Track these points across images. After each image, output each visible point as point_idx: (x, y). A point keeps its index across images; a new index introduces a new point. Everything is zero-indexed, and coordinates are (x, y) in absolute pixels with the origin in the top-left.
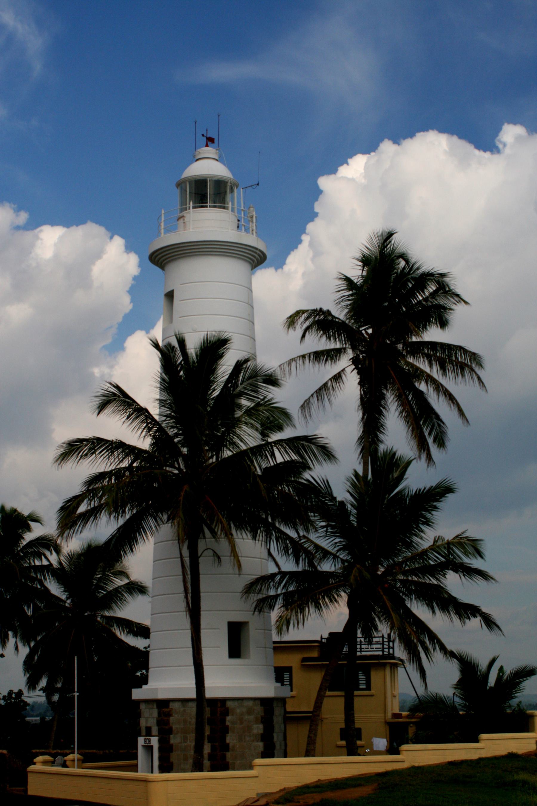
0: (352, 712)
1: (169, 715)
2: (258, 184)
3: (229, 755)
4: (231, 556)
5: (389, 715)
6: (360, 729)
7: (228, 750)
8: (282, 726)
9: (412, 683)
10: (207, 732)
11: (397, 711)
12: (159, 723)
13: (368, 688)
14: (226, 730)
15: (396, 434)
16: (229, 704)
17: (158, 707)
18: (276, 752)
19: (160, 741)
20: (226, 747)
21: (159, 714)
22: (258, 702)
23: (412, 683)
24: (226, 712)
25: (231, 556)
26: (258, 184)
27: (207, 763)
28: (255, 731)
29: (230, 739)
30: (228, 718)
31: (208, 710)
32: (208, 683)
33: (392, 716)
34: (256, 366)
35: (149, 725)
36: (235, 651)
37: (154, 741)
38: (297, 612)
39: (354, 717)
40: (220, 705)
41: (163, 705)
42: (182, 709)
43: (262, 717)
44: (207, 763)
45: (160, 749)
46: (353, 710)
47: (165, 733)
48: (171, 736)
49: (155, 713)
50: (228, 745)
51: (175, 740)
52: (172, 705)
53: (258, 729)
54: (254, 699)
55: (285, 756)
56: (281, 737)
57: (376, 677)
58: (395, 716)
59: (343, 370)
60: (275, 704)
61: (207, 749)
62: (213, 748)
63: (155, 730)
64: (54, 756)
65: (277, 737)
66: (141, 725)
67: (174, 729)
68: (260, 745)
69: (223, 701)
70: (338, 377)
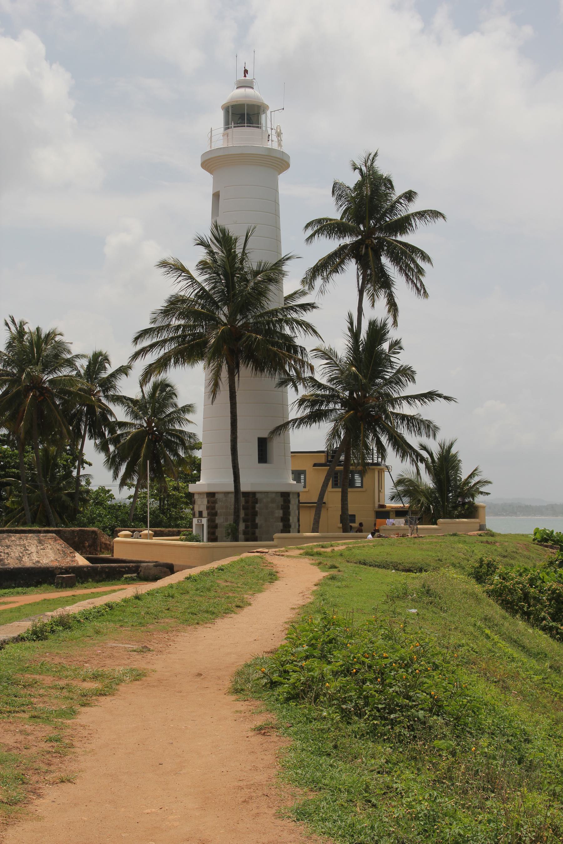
1: (215, 502)
3: (257, 531)
5: (377, 505)
7: (257, 528)
8: (297, 512)
10: (242, 514)
12: (208, 508)
14: (255, 514)
16: (258, 496)
17: (207, 497)
18: (291, 530)
19: (208, 521)
20: (255, 526)
21: (208, 502)
24: (256, 501)
27: (241, 536)
28: (277, 515)
29: (258, 520)
30: (257, 506)
31: (242, 499)
32: (242, 480)
35: (201, 510)
36: (263, 457)
37: (204, 521)
40: (251, 498)
41: (211, 495)
42: (224, 499)
43: (282, 505)
44: (241, 536)
45: (209, 527)
47: (212, 514)
48: (217, 517)
49: (205, 501)
50: (257, 524)
51: (219, 520)
52: (216, 495)
53: (279, 513)
54: (277, 493)
55: (299, 532)
56: (296, 520)
60: (291, 496)
61: (242, 526)
62: (247, 527)
63: (205, 514)
64: (133, 532)
65: (293, 519)
68: (281, 524)
69: (254, 494)
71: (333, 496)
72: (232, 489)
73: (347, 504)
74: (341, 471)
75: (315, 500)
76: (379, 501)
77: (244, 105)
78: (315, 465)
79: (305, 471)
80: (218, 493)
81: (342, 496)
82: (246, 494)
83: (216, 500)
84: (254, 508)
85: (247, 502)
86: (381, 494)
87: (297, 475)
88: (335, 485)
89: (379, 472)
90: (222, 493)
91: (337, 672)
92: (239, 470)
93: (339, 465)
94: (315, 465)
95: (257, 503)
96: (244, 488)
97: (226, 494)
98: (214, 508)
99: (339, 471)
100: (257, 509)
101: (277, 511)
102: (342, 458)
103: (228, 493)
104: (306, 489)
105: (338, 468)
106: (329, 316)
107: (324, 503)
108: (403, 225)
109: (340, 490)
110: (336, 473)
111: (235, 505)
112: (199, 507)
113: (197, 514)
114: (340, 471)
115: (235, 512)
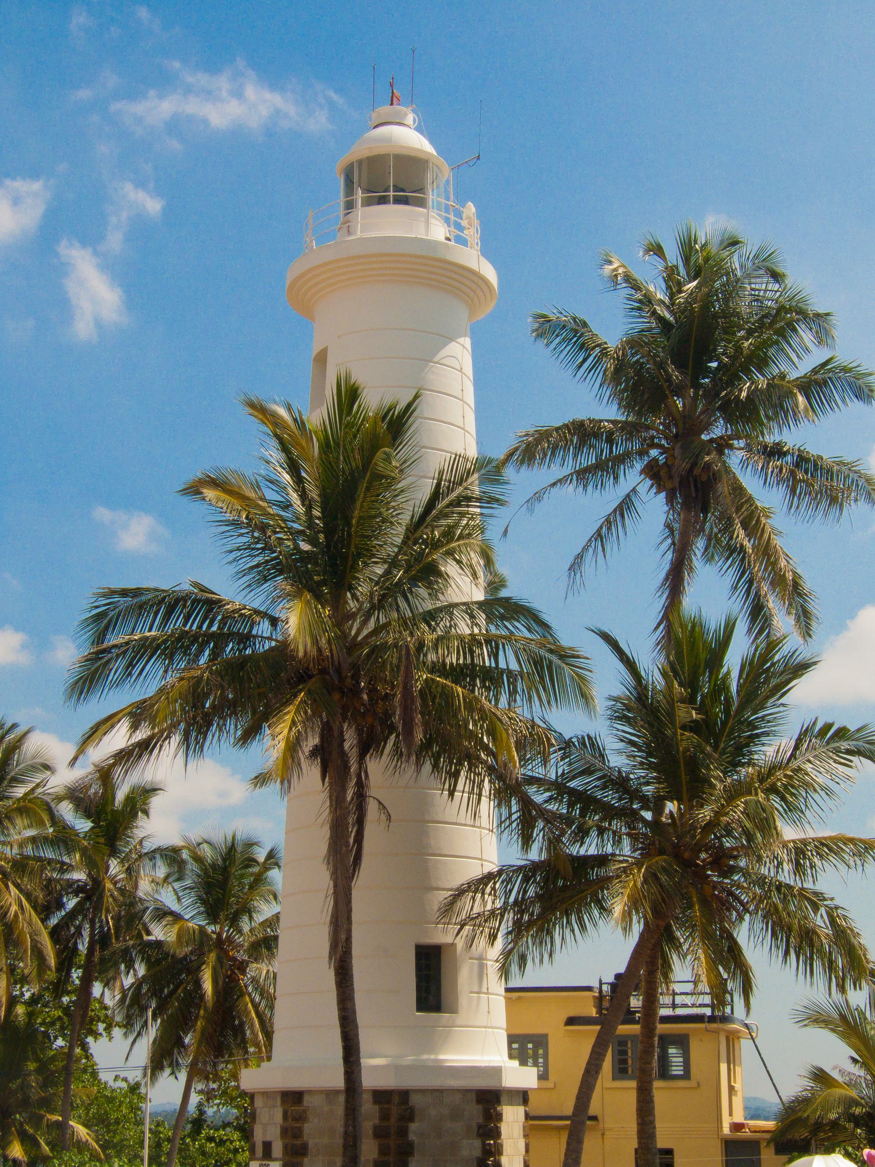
0: (650, 1118)
1: (301, 1118)
2: (478, 158)
4: (497, 961)
5: (726, 1130)
6: (669, 1152)
8: (522, 1144)
9: (768, 1071)
11: (738, 1118)
12: (284, 1132)
13: (686, 1076)
15: (712, 595)
17: (283, 1102)
22: (474, 1096)
23: (766, 1067)
24: (409, 1116)
25: (497, 961)
26: (478, 158)
28: (465, 1153)
30: (413, 1126)
33: (730, 1128)
34: (605, 910)
35: (268, 1139)
38: (438, 662)
39: (655, 1128)
41: (293, 1098)
42: (326, 1109)
43: (480, 1127)
46: (653, 1115)
48: (306, 1160)
52: (307, 1100)
54: (466, 1092)
57: (700, 1049)
58: (737, 1127)
59: (634, 490)
63: (277, 1149)
66: (255, 1139)
67: (310, 1146)
69: (404, 1095)
70: (625, 507)
71: (616, 1099)
72: (338, 1081)
73: (652, 1122)
74: (635, 1036)
75: (569, 1110)
76: (731, 1114)
77: (389, 155)
78: (571, 1021)
79: (545, 1036)
80: (310, 1092)
81: (639, 1101)
82: (381, 1096)
83: (305, 1111)
84: (403, 1132)
85: (385, 1116)
86: (81, 757)
87: (524, 1046)
88: (621, 1072)
89: (728, 1039)
90: (322, 1092)
91: (705, 903)
92: (356, 1027)
93: (625, 1022)
94: (571, 1021)
95: (411, 1119)
96: (369, 1081)
97: (330, 1094)
98: (297, 1133)
99: (629, 1036)
100: (412, 1137)
101: (465, 1142)
102: (636, 1002)
103: (337, 1092)
104: (549, 1084)
105: (623, 1029)
106: (582, 581)
107: (594, 1118)
108: (777, 401)
109: (633, 1084)
110: (622, 1042)
111: (346, 1126)
112: (265, 1132)
113: (259, 1151)
114: (632, 1037)
115: (345, 1147)
